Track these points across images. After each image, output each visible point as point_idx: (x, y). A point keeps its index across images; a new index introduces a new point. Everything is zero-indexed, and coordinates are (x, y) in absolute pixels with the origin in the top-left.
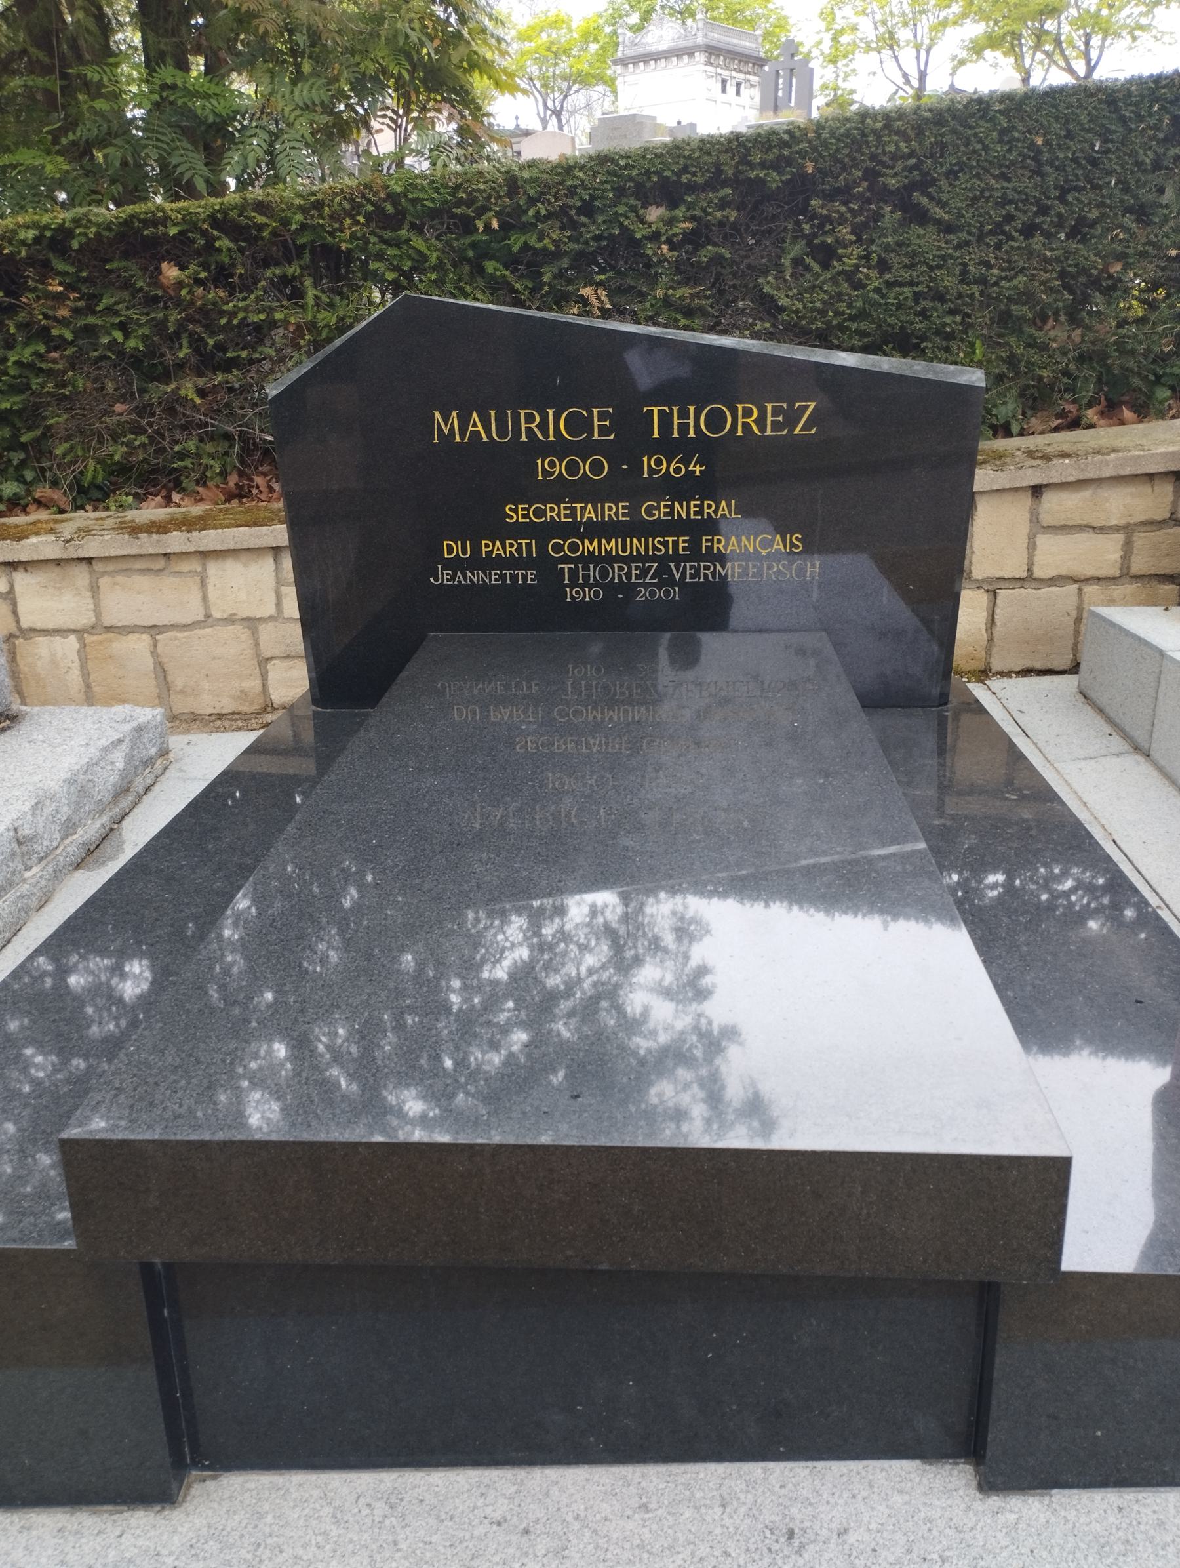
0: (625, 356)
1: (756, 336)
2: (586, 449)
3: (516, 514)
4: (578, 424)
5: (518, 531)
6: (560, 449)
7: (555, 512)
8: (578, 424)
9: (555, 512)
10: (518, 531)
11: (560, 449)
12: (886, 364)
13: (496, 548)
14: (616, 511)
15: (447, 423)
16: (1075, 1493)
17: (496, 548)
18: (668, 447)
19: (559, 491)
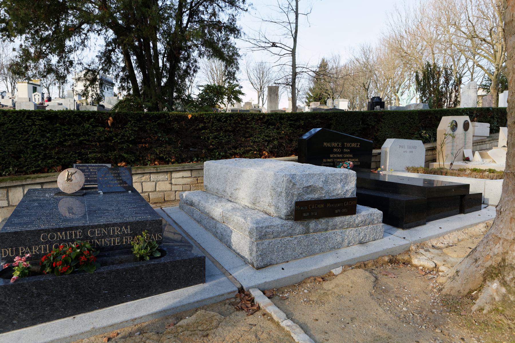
0: (488, 125)
1: (93, 163)
2: (339, 148)
3: (331, 156)
4: (338, 145)
5: (331, 158)
6: (336, 148)
7: (335, 156)
8: (338, 145)
9: (335, 156)
10: (331, 158)
11: (336, 148)
12: (104, 165)
13: (329, 160)
14: (341, 156)
15: (325, 144)
16: (431, 222)
17: (329, 160)
18: (347, 148)
19: (336, 153)
